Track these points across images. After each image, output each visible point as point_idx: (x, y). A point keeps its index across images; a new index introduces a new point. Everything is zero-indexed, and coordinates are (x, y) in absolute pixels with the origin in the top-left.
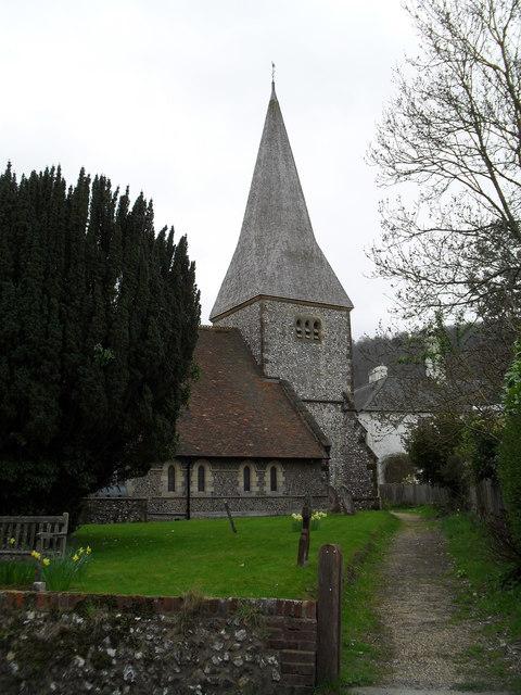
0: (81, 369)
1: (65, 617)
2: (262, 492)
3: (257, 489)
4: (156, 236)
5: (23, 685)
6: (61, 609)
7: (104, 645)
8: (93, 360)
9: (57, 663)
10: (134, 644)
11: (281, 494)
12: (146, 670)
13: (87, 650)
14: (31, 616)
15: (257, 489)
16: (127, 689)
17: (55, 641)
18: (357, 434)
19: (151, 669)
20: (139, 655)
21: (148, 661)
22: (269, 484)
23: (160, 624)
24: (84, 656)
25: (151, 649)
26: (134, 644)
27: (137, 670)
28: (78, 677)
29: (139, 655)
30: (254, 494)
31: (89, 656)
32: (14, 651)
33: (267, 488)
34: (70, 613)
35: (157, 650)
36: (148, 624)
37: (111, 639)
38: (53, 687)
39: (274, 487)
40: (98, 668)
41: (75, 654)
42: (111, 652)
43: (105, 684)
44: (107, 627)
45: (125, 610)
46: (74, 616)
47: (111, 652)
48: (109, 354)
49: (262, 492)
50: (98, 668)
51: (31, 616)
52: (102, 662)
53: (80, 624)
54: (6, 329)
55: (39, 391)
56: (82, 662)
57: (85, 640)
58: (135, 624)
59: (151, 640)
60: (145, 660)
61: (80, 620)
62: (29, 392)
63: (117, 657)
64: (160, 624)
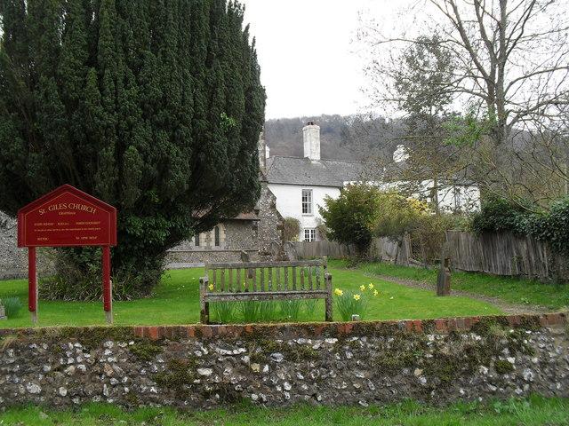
0: (208, 134)
1: (465, 336)
2: (209, 247)
3: (205, 244)
4: (243, 30)
5: (433, 393)
6: (458, 330)
7: (503, 355)
8: (219, 126)
9: (463, 373)
10: (530, 352)
11: (223, 249)
12: (542, 371)
13: (489, 360)
14: (431, 338)
15: (205, 244)
16: (526, 387)
17: (461, 355)
18: (269, 201)
19: (546, 370)
20: (535, 360)
21: (543, 364)
22: (214, 240)
23: (549, 334)
24: (487, 365)
25: (545, 354)
26: (530, 352)
27: (535, 371)
28: (483, 382)
29: (535, 360)
30: (203, 249)
31: (492, 364)
32: (420, 367)
33: (213, 243)
34: (468, 333)
35: (551, 354)
36: (538, 335)
37: (510, 349)
38: (462, 391)
39: (217, 243)
40: (501, 373)
41: (480, 364)
42: (511, 360)
43: (508, 385)
44: (504, 341)
45: (516, 326)
46: (473, 335)
47: (511, 360)
48: (232, 121)
49: (209, 247)
50: (501, 373)
51: (431, 338)
52: (503, 368)
53: (479, 341)
54: (152, 93)
55: (177, 153)
56: (486, 370)
57: (490, 351)
58: (526, 337)
59: (544, 348)
60: (540, 363)
61: (478, 338)
62: (168, 153)
63: (516, 364)
64: (549, 334)
